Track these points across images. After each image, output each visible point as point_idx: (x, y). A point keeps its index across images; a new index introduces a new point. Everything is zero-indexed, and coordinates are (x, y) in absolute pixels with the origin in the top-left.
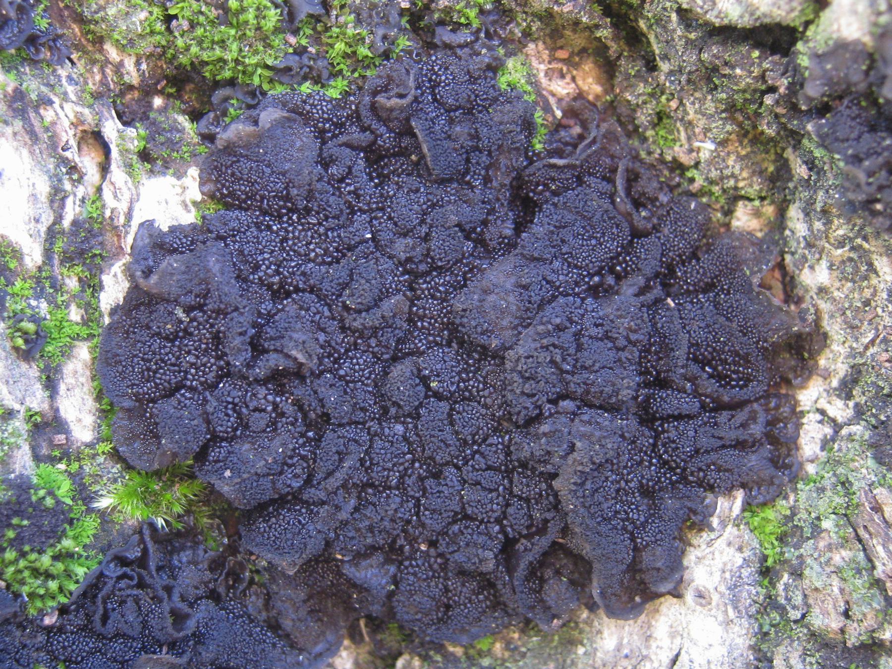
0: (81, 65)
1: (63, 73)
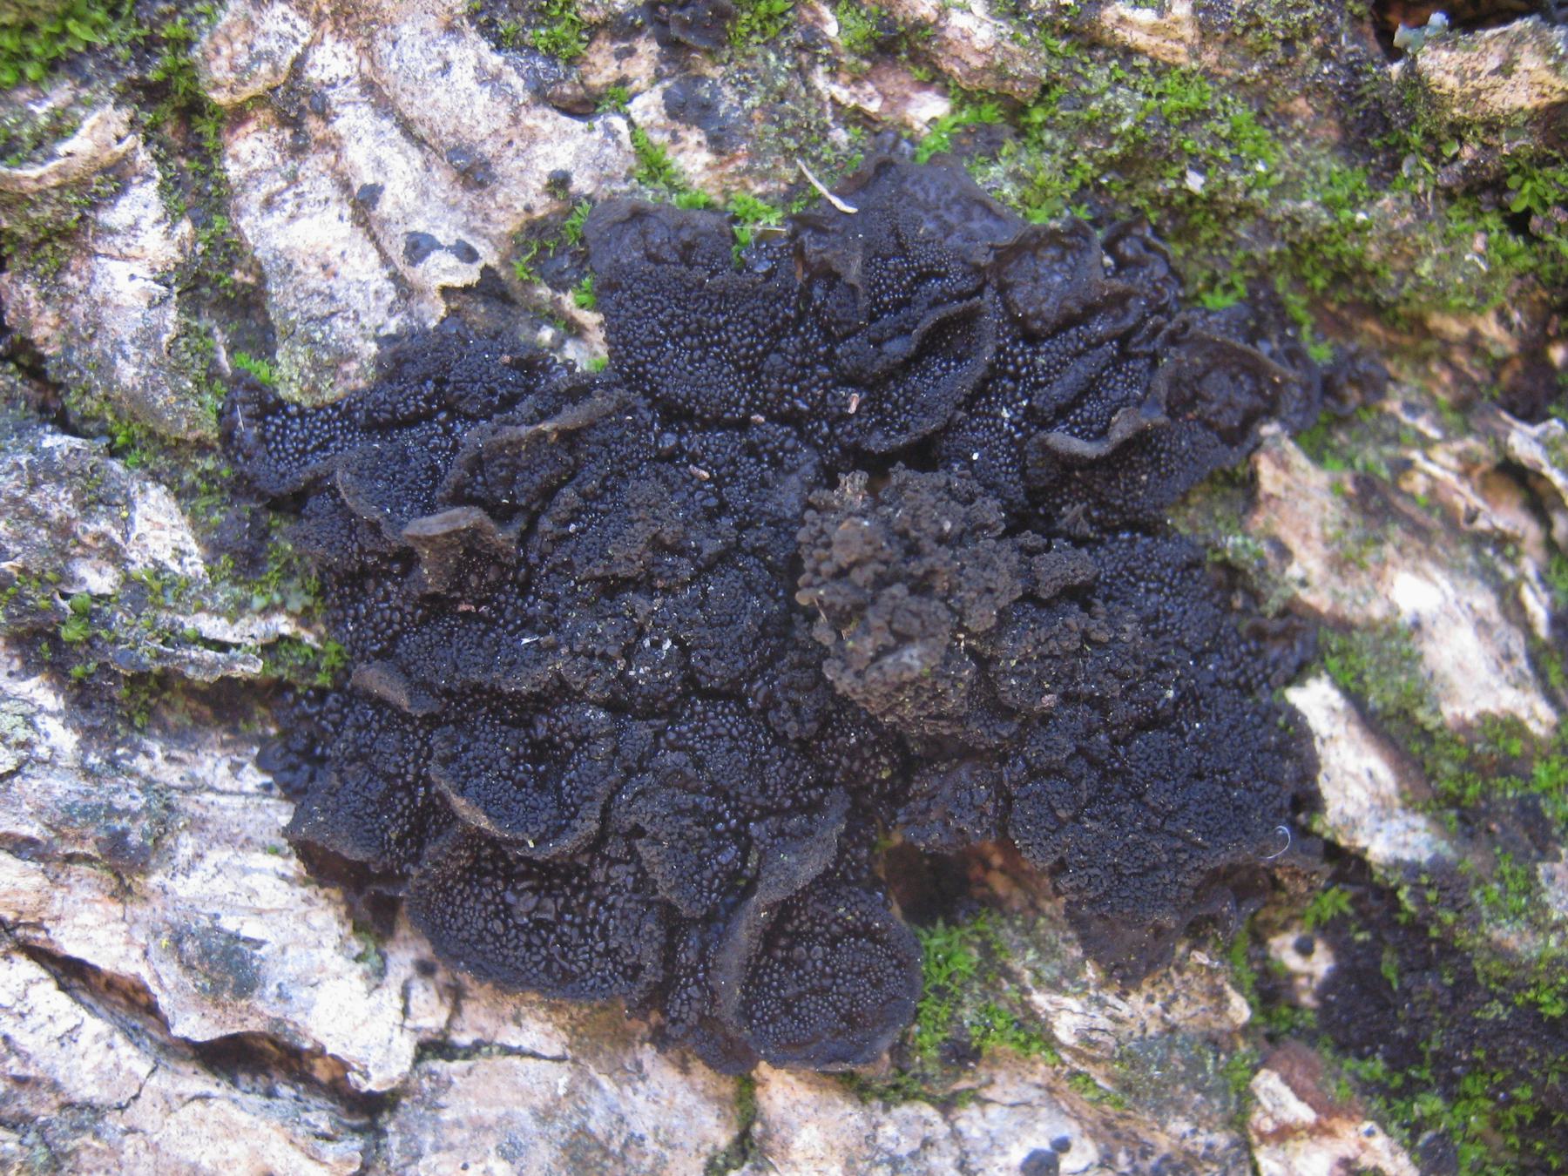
0: (1406, 374)
1: (1393, 405)
